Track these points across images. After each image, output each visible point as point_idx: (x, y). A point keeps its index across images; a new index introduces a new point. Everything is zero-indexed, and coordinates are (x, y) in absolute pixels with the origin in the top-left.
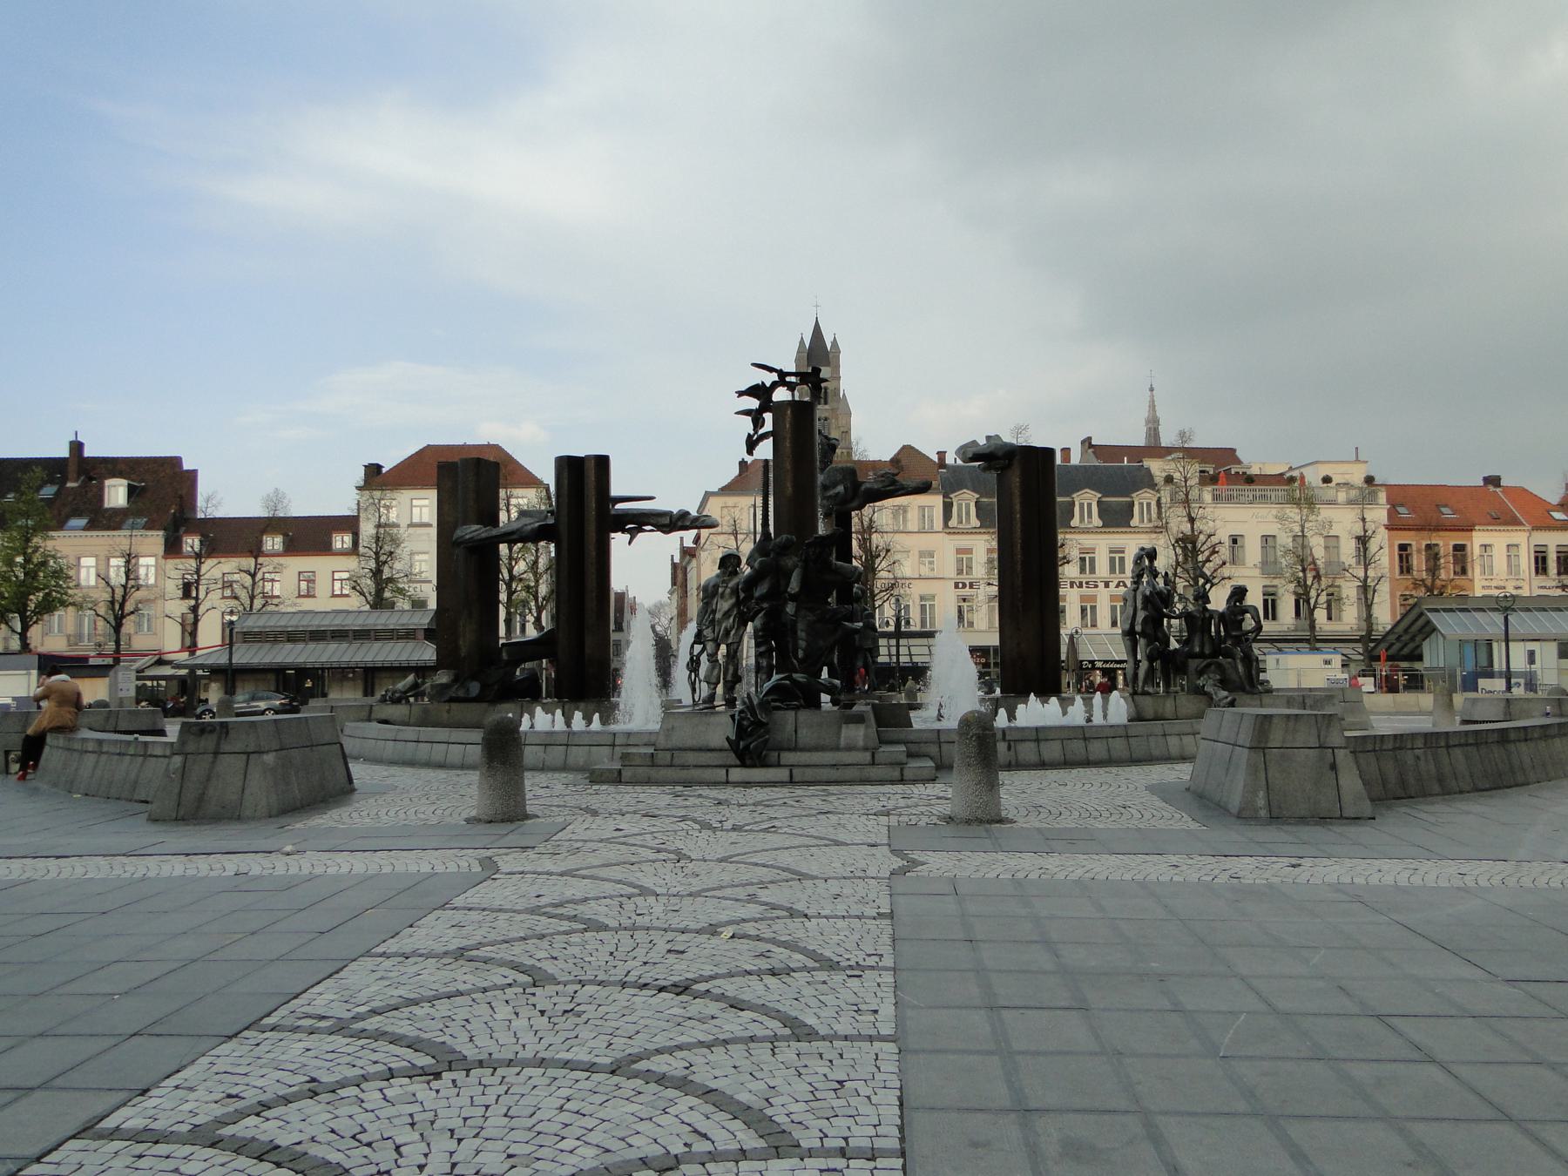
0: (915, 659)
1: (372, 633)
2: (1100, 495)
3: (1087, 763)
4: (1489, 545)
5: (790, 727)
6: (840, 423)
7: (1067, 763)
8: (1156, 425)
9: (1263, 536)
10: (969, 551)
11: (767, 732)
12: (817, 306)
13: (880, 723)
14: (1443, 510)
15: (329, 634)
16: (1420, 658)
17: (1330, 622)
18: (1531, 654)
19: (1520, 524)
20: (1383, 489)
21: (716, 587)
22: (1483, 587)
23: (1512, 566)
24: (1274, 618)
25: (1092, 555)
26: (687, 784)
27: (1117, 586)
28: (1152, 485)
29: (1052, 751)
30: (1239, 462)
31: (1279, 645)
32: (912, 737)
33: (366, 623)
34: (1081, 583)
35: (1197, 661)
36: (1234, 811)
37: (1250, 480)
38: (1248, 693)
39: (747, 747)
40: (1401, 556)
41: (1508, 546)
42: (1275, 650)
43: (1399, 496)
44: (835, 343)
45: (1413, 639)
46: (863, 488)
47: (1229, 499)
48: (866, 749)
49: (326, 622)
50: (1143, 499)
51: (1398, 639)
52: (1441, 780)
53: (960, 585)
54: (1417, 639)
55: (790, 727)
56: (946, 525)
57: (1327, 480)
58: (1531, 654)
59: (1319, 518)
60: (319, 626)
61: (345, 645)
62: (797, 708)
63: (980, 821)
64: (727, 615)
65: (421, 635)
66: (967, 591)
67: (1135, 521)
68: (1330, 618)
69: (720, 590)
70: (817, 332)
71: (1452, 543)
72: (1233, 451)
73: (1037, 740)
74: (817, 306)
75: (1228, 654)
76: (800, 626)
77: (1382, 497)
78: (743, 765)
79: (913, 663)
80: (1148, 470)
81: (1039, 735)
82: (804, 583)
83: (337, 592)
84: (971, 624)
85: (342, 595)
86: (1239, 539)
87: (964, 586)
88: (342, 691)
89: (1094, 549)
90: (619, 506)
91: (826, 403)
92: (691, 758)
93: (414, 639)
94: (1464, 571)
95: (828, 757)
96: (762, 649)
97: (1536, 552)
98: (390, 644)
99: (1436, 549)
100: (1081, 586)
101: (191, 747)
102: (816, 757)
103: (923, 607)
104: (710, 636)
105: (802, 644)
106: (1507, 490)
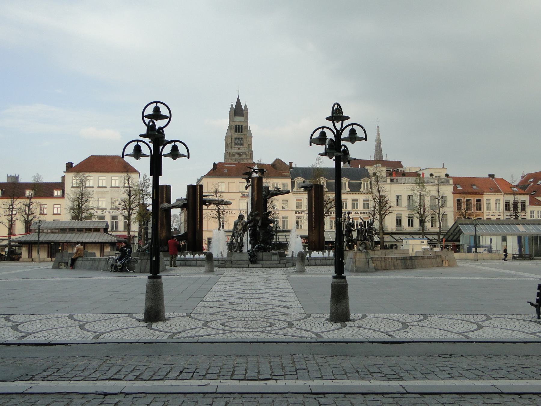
0: (280, 240)
1: (84, 230)
2: (304, 179)
3: (326, 265)
4: (489, 200)
5: (261, 256)
6: (248, 140)
7: (321, 265)
8: (380, 142)
9: (408, 196)
10: (301, 200)
11: (256, 257)
12: (238, 91)
13: (280, 256)
14: (473, 186)
15: (68, 230)
16: (459, 241)
17: (432, 227)
18: (491, 240)
19: (501, 192)
20: (452, 179)
21: (238, 223)
22: (487, 215)
23: (497, 208)
24: (412, 226)
25: (357, 202)
26: (241, 268)
27: (355, 214)
28: (368, 176)
29: (318, 262)
30: (402, 167)
31: (413, 236)
32: (287, 259)
33: (82, 226)
34: (361, 214)
35: (360, 242)
36: (350, 270)
37: (404, 174)
38: (372, 250)
39: (253, 260)
40: (458, 203)
41: (496, 200)
42: (412, 238)
43: (457, 181)
44: (246, 107)
45: (456, 234)
46: (271, 192)
47: (396, 182)
48: (277, 261)
49: (66, 225)
50: (365, 182)
51: (451, 234)
52: (394, 266)
53: (297, 213)
54: (458, 234)
55: (261, 256)
56: (292, 190)
57: (432, 175)
58: (491, 240)
59: (426, 190)
60: (64, 227)
61: (74, 234)
62: (262, 252)
63: (301, 272)
64: (240, 230)
65: (102, 230)
66: (300, 215)
67: (362, 190)
68: (432, 226)
69: (239, 224)
70: (238, 102)
71: (456, 198)
72: (400, 162)
73: (315, 260)
74: (238, 91)
75: (367, 240)
76: (261, 233)
77: (451, 181)
78: (252, 264)
79: (279, 242)
80: (367, 170)
81: (315, 259)
82: (262, 223)
83: (55, 212)
84: (301, 227)
85: (57, 214)
86: (400, 197)
87: (299, 213)
88: (92, 249)
89: (347, 200)
90: (204, 198)
91: (242, 132)
92: (240, 262)
93: (100, 232)
94: (480, 209)
95: (269, 262)
96: (251, 239)
97: (506, 202)
98: (91, 234)
99: (470, 202)
100: (364, 214)
101: (142, 258)
102: (267, 262)
103: (283, 221)
104: (236, 235)
105: (261, 237)
106: (497, 179)
